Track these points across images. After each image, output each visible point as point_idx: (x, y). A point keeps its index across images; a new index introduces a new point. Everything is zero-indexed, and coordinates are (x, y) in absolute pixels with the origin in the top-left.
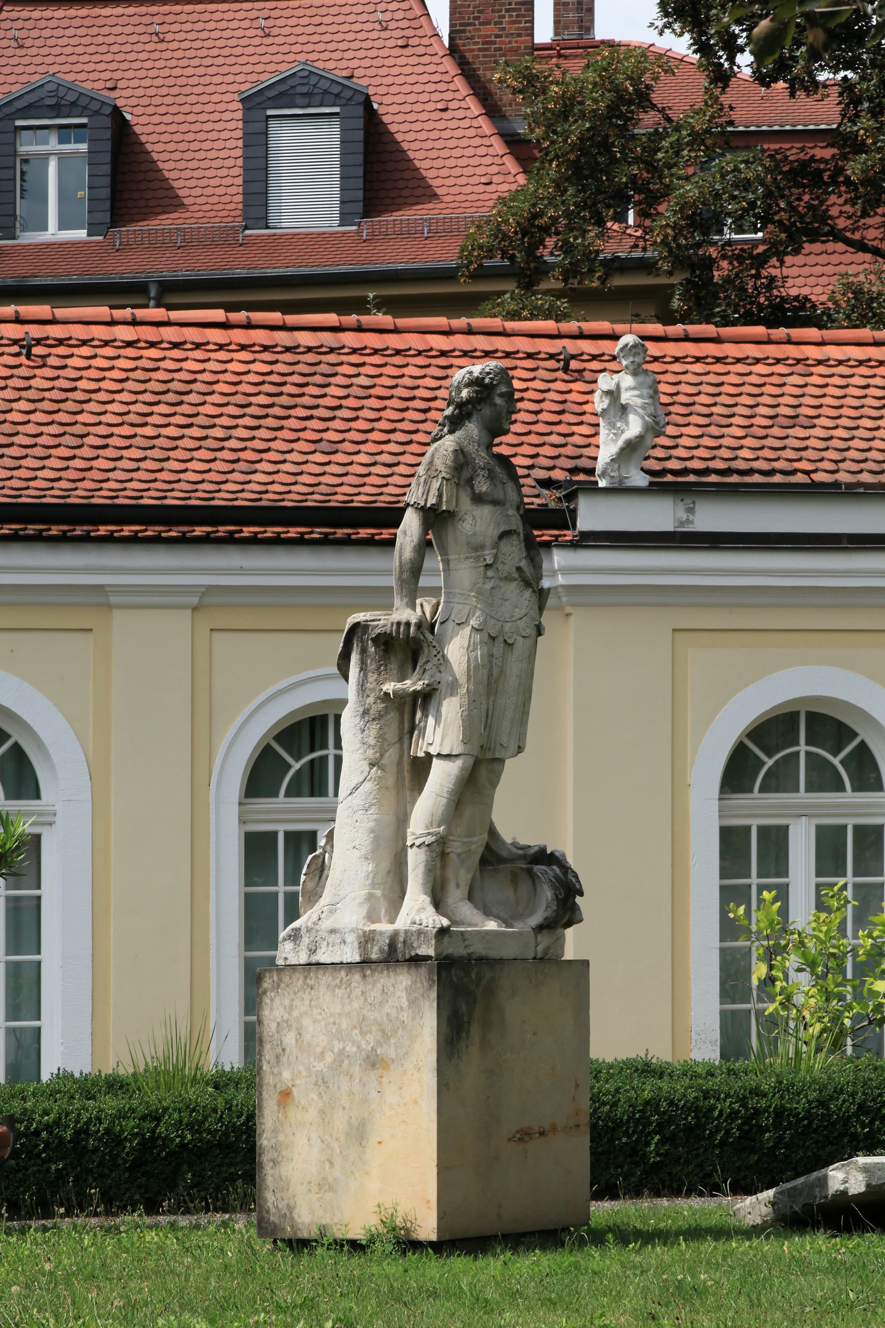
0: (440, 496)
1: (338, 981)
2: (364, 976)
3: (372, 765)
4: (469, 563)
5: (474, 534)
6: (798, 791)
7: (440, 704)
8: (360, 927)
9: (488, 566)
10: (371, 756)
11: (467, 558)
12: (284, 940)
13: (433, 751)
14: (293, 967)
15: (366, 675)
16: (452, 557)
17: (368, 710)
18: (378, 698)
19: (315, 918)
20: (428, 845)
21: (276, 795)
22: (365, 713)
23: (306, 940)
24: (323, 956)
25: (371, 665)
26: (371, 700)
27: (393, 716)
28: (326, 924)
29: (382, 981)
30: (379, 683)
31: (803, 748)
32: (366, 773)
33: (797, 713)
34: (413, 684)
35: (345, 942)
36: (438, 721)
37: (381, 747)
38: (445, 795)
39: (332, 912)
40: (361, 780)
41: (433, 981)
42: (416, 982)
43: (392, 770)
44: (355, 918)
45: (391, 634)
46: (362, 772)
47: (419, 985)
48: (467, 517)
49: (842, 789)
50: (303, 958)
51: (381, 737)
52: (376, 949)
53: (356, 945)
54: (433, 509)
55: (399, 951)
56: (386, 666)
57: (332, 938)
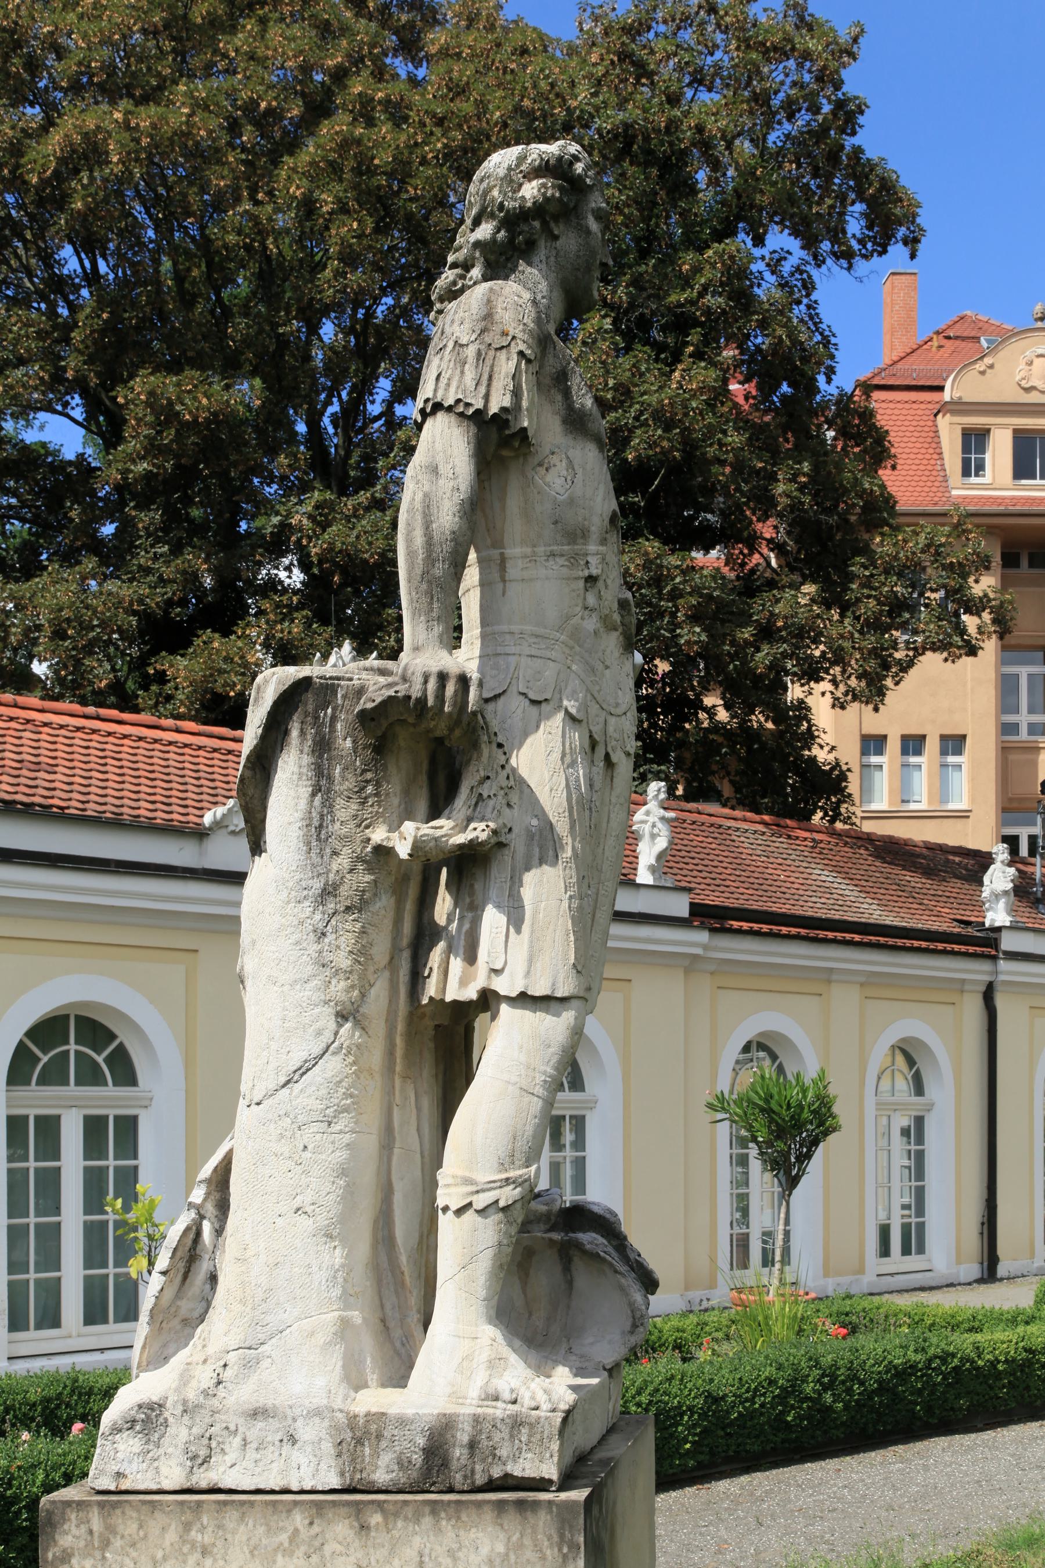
0: (516, 393)
1: (284, 1537)
2: (364, 1528)
3: (342, 1017)
4: (557, 567)
5: (571, 502)
6: (68, 1084)
7: (516, 882)
8: (338, 1404)
9: (591, 580)
10: (343, 997)
11: (553, 555)
12: (116, 1430)
13: (503, 986)
14: (151, 1497)
15: (328, 804)
16: (514, 551)
17: (336, 886)
18: (359, 859)
19: (205, 1377)
20: (505, 1209)
21: (29, 1084)
22: (328, 892)
23: (179, 1433)
24: (225, 1472)
25: (343, 781)
26: (343, 862)
27: (385, 903)
28: (241, 1394)
29: (417, 1541)
30: (363, 824)
31: (72, 1047)
32: (328, 1036)
33: (67, 1016)
34: (451, 831)
35: (293, 1440)
36: (516, 918)
37: (362, 977)
38: (539, 1090)
39: (249, 1365)
40: (317, 1051)
41: (573, 1546)
42: (520, 1546)
43: (378, 1028)
44: (321, 1382)
45: (422, 701)
46: (319, 1033)
47: (529, 1554)
48: (554, 459)
49: (106, 1085)
50: (172, 1476)
51: (362, 953)
52: (386, 1459)
53: (328, 1447)
54: (501, 420)
55: (454, 1465)
56: (378, 785)
57: (256, 1430)
